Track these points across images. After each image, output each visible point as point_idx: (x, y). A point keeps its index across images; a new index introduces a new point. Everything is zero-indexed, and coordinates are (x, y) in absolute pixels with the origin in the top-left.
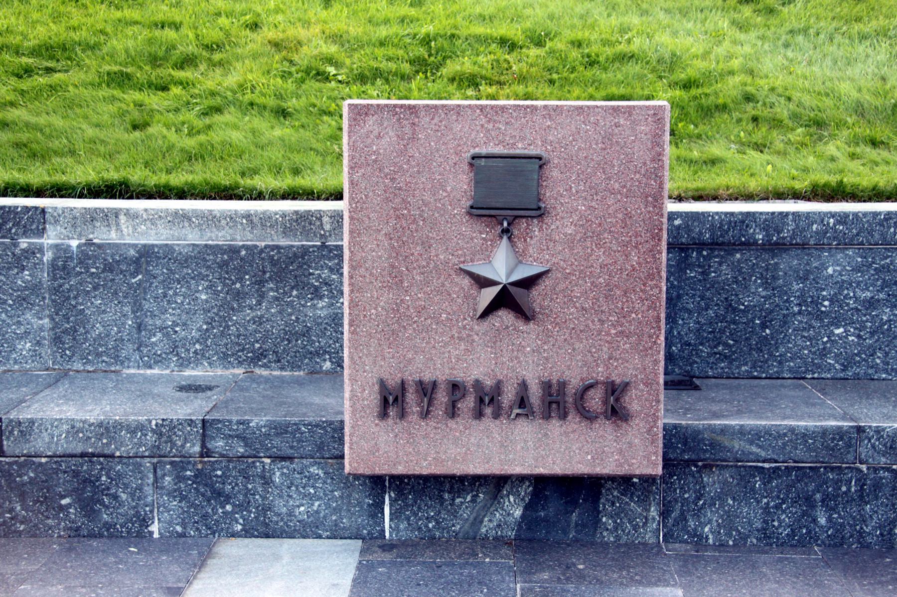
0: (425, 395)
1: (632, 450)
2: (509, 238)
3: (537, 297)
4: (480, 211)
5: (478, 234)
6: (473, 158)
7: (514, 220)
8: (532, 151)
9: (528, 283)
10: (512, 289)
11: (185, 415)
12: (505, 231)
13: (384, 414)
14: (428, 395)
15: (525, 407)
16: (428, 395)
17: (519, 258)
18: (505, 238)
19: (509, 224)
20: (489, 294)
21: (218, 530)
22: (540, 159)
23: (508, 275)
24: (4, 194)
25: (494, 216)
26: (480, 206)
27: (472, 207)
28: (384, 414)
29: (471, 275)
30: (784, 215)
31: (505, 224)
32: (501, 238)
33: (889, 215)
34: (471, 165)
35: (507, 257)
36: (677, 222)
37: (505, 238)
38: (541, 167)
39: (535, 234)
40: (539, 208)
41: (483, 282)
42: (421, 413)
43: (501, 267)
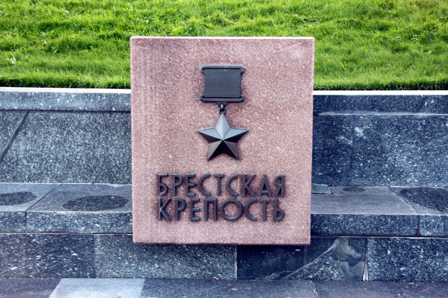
1: (294, 230)
2: (224, 114)
3: (243, 145)
4: (206, 100)
6: (203, 69)
7: (227, 104)
9: (236, 139)
10: (226, 143)
12: (222, 110)
13: (281, 179)
17: (231, 125)
18: (222, 114)
19: (224, 106)
20: (216, 145)
21: (248, 212)
23: (224, 138)
25: (215, 102)
26: (219, 96)
27: (203, 97)
28: (281, 179)
30: (324, 97)
31: (222, 106)
32: (221, 114)
33: (447, 97)
34: (203, 73)
37: (222, 114)
38: (242, 74)
40: (241, 97)
41: (210, 139)
43: (221, 131)
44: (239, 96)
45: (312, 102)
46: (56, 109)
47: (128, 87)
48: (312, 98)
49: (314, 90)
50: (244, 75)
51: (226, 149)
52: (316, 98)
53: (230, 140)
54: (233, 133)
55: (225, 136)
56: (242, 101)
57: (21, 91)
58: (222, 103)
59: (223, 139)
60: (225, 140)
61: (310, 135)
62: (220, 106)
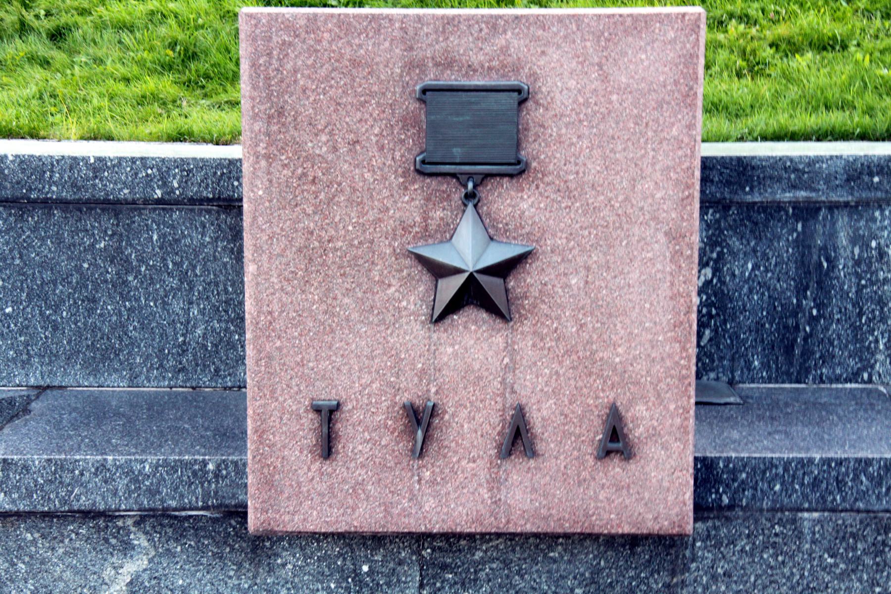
0: (419, 422)
1: (657, 492)
2: (475, 206)
3: (526, 282)
4: (426, 169)
5: (441, 202)
6: (424, 91)
7: (483, 180)
8: (513, 82)
9: (504, 269)
10: (475, 274)
11: (262, 418)
14: (424, 423)
15: (618, 441)
16: (424, 423)
17: (492, 233)
18: (470, 206)
20: (450, 286)
22: (519, 91)
24: (8, 134)
25: (453, 175)
27: (423, 162)
29: (422, 260)
31: (470, 185)
32: (465, 205)
35: (474, 238)
36: (238, 164)
37: (470, 206)
38: (522, 102)
39: (508, 201)
41: (439, 271)
42: (413, 451)
43: (468, 249)
44: (513, 161)
45: (692, 464)
46: (506, 180)
47: (232, 139)
48: (698, 164)
49: (703, 141)
50: (530, 104)
51: (481, 295)
52: (707, 164)
53: (488, 271)
54: (497, 254)
55: (478, 260)
56: (522, 172)
57: (199, 155)
58: (470, 176)
59: (471, 270)
60: (480, 271)
61: (688, 358)
62: (465, 186)
